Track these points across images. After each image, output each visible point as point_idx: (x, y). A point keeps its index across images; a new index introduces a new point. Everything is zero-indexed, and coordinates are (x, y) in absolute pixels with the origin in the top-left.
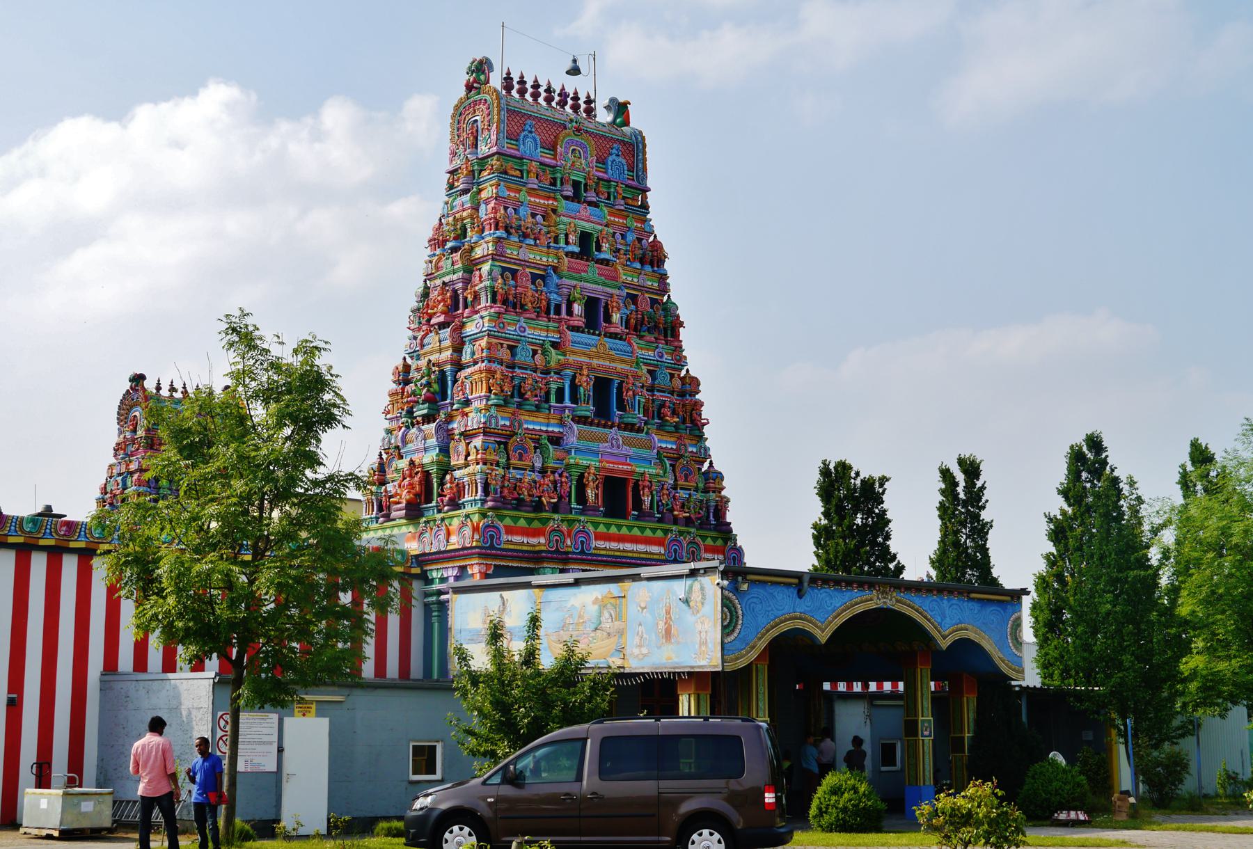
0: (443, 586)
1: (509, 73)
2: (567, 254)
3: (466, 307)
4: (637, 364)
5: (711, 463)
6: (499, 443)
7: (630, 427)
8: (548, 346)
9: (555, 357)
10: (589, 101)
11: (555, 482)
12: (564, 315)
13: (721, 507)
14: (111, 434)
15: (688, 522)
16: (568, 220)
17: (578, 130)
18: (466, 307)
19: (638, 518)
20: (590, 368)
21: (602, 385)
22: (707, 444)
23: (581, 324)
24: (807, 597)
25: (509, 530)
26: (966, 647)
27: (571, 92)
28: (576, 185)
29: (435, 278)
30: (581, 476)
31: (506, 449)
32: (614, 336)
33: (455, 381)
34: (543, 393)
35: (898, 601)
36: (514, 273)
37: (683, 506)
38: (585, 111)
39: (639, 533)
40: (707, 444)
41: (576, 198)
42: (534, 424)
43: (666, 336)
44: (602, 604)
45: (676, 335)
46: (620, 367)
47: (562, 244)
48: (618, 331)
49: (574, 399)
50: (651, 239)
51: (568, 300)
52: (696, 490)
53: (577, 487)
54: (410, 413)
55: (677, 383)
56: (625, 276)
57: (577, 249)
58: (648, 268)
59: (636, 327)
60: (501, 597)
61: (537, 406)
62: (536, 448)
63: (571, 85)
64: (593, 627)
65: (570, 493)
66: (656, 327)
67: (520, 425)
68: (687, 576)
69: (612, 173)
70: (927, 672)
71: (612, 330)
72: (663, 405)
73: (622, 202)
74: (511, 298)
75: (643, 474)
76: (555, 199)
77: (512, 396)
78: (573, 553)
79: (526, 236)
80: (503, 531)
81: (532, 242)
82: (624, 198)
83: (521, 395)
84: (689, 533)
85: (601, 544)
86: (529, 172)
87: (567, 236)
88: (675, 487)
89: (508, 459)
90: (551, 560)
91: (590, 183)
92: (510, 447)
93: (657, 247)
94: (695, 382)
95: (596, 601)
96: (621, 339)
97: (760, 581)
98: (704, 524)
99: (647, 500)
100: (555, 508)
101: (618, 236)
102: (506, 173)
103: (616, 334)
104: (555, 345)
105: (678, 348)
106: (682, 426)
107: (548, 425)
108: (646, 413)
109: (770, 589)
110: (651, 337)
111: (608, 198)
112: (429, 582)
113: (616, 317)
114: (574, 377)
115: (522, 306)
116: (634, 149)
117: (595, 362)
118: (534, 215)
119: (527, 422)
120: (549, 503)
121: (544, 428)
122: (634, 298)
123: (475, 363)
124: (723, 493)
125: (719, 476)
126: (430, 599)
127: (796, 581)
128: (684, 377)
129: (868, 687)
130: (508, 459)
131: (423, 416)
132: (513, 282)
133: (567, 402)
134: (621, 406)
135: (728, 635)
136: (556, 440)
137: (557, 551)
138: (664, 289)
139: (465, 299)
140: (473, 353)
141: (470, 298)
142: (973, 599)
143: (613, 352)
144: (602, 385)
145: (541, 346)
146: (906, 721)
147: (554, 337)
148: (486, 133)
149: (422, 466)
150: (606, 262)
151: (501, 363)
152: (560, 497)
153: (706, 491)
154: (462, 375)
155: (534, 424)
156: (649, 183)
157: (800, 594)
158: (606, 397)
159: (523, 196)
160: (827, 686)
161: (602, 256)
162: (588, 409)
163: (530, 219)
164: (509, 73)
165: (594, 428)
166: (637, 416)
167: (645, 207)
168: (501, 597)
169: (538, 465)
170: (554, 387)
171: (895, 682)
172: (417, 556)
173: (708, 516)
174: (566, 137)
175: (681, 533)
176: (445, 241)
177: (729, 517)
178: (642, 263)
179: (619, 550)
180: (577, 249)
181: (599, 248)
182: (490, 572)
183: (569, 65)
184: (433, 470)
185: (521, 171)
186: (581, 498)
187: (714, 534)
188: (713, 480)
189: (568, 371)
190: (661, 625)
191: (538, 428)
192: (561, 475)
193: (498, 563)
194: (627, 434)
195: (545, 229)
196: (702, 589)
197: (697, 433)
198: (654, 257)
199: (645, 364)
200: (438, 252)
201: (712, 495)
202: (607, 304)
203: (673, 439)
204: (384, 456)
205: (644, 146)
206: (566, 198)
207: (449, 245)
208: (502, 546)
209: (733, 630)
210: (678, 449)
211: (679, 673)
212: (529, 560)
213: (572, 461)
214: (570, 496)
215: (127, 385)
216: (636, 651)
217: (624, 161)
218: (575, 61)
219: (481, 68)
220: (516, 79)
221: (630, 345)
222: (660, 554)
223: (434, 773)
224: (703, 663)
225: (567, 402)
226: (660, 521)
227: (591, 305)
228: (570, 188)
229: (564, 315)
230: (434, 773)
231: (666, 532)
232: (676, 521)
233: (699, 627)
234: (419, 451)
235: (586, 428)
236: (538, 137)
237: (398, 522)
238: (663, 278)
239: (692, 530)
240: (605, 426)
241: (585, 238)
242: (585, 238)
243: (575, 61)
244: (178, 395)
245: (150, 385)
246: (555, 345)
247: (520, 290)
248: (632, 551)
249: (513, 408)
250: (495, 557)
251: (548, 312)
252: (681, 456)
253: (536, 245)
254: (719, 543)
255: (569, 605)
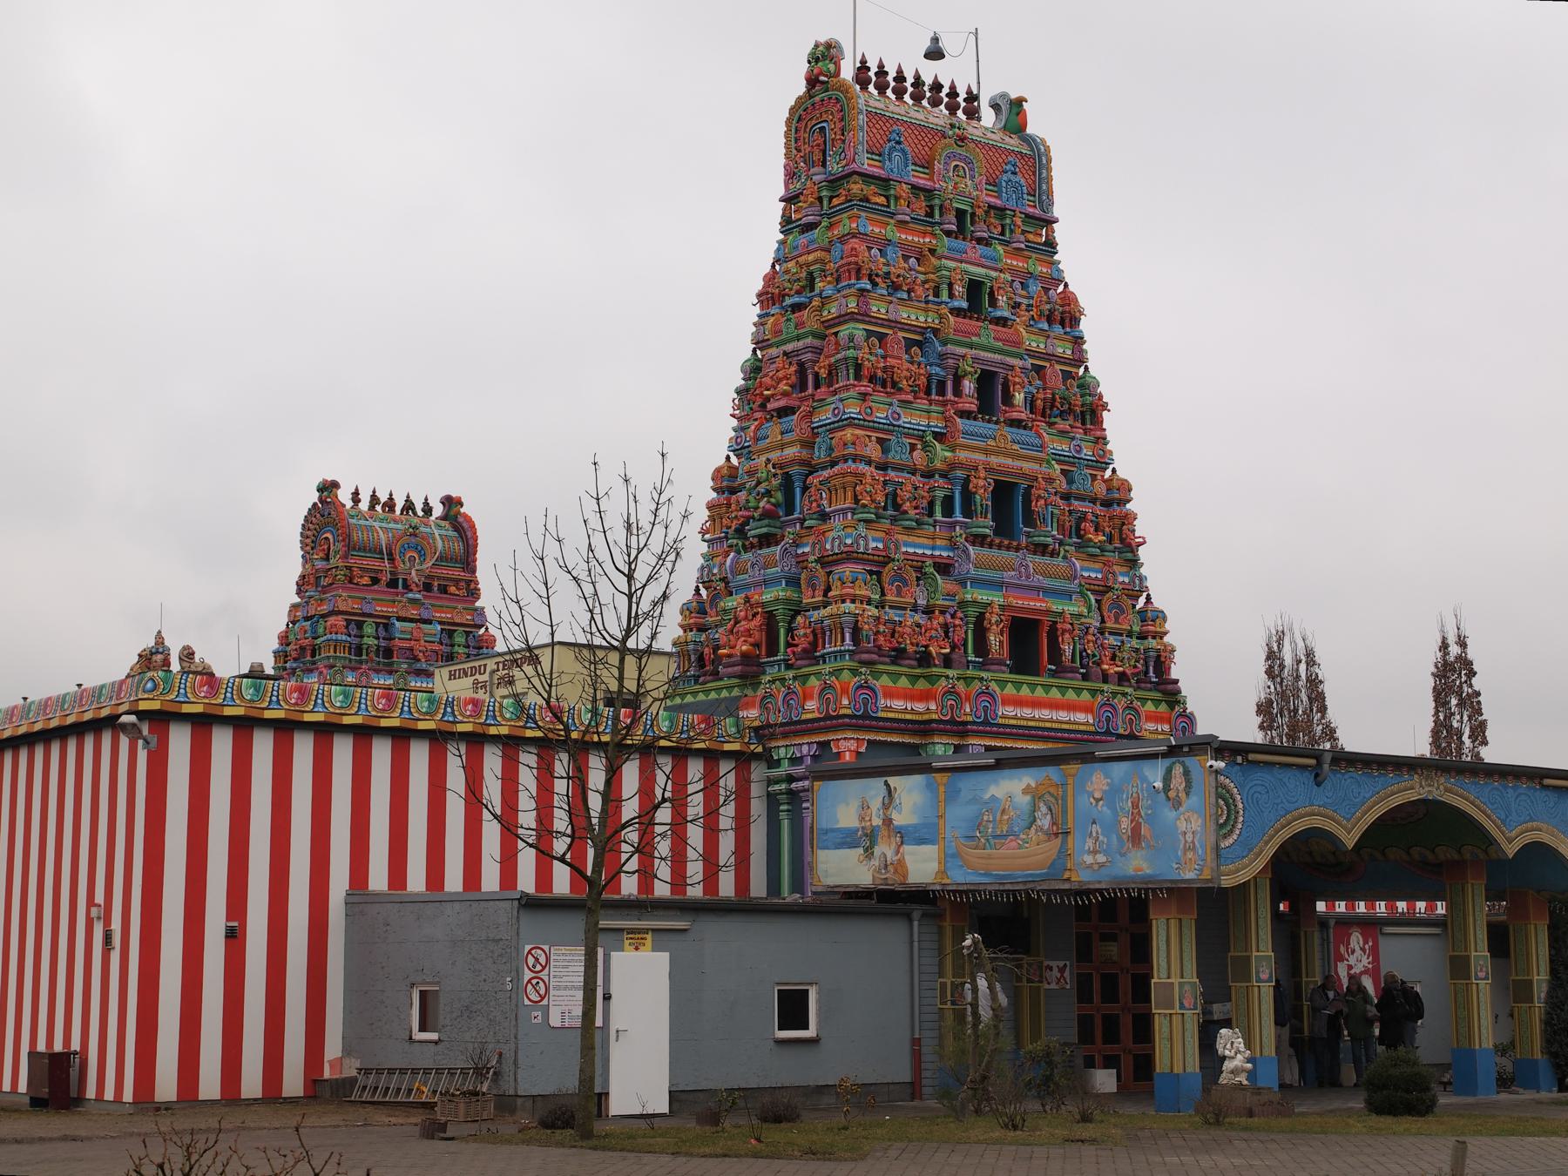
0: (799, 770)
1: (863, 62)
2: (952, 311)
3: (817, 386)
4: (1048, 462)
5: (1148, 598)
6: (871, 573)
7: (1041, 549)
8: (929, 438)
9: (942, 452)
10: (972, 98)
11: (945, 627)
12: (950, 396)
13: (1161, 662)
14: (292, 564)
15: (1122, 678)
16: (952, 264)
17: (962, 139)
18: (817, 386)
19: (1054, 674)
20: (989, 470)
21: (1003, 491)
22: (1143, 571)
23: (974, 408)
24: (1328, 784)
25: (889, 694)
26: (1537, 852)
27: (928, 80)
28: (960, 214)
29: (770, 346)
30: (981, 618)
31: (879, 581)
32: (1016, 423)
33: (805, 489)
34: (925, 503)
35: (1447, 790)
36: (881, 337)
37: (1113, 658)
38: (912, 97)
39: (1059, 696)
40: (1143, 571)
41: (960, 232)
42: (914, 546)
43: (1084, 423)
44: (1036, 795)
45: (1098, 422)
46: (1027, 466)
47: (945, 296)
48: (1023, 416)
49: (968, 511)
50: (1061, 288)
51: (956, 375)
52: (1130, 635)
53: (974, 631)
54: (741, 532)
55: (1100, 489)
56: (1034, 343)
57: (965, 305)
58: (1058, 329)
59: (1048, 410)
60: (886, 783)
61: (917, 521)
62: (918, 579)
63: (929, 71)
64: (1024, 824)
65: (966, 640)
66: (1071, 411)
67: (897, 548)
68: (1164, 755)
69: (1006, 200)
70: (1481, 891)
71: (1015, 415)
72: (1083, 518)
73: (1022, 238)
74: (880, 374)
75: (1061, 614)
76: (933, 235)
77: (885, 508)
78: (974, 723)
79: (895, 287)
80: (880, 695)
81: (905, 296)
82: (1024, 232)
83: (897, 507)
84: (1124, 694)
85: (1010, 711)
86: (897, 198)
87: (950, 286)
88: (1102, 631)
89: (883, 594)
90: (944, 732)
91: (979, 212)
92: (886, 579)
93: (1069, 299)
94: (1126, 487)
95: (1026, 791)
96: (1025, 428)
97: (1266, 763)
98: (1141, 681)
99: (1067, 649)
100: (947, 662)
101: (1017, 285)
102: (868, 200)
103: (1020, 421)
104: (939, 437)
105: (1101, 440)
106: (1110, 547)
107: (933, 548)
108: (1061, 528)
109: (1276, 770)
110: (1063, 425)
111: (1003, 234)
112: (773, 764)
113: (1019, 398)
114: (967, 481)
115: (894, 384)
116: (1033, 163)
117: (994, 460)
118: (906, 258)
119: (906, 545)
120: (939, 654)
121: (929, 552)
122: (1039, 370)
123: (833, 464)
124: (1166, 639)
125: (1160, 616)
126: (777, 787)
127: (1313, 762)
128: (1110, 480)
129: (1373, 908)
130: (883, 594)
131: (760, 536)
132: (880, 351)
133: (958, 516)
134: (1029, 519)
135: (1225, 837)
136: (944, 568)
137: (986, 723)
138: (1079, 359)
139: (816, 375)
140: (831, 449)
141: (823, 373)
142: (1547, 787)
143: (1016, 447)
144: (1003, 491)
145: (921, 438)
146: (1452, 958)
147: (938, 424)
148: (839, 144)
149: (763, 605)
150: (1002, 322)
151: (869, 463)
152: (953, 647)
153: (1142, 637)
154: (814, 480)
155: (914, 546)
156: (1057, 211)
157: (1318, 780)
158: (1009, 504)
159: (892, 232)
160: (1321, 906)
161: (999, 314)
162: (985, 526)
163: (903, 264)
164: (863, 62)
165: (995, 552)
166: (1049, 533)
167: (1051, 245)
168: (886, 783)
169: (922, 602)
170: (940, 494)
171: (1431, 898)
172: (756, 729)
173: (1147, 672)
174: (946, 148)
175: (1114, 694)
176: (783, 296)
177: (1175, 673)
178: (1050, 320)
179: (1033, 719)
180: (965, 305)
181: (993, 302)
182: (862, 750)
183: (926, 44)
184: (780, 610)
185: (887, 198)
186: (981, 647)
187: (1158, 695)
188: (1152, 622)
189: (959, 473)
190: (1125, 823)
191: (920, 551)
192: (953, 616)
193: (872, 737)
194: (1038, 559)
195: (922, 277)
196: (1186, 773)
197: (1129, 556)
198: (1066, 315)
199: (1059, 462)
200: (775, 310)
201: (1152, 643)
202: (1006, 379)
203: (1097, 566)
204: (703, 592)
205: (1049, 160)
206: (948, 233)
207: (788, 301)
208: (1001, 721)
209: (1231, 831)
210: (1105, 578)
211: (1154, 890)
212: (914, 733)
213: (969, 597)
214: (965, 645)
215: (314, 497)
216: (1089, 859)
217: (1023, 181)
218: (935, 40)
219: (825, 54)
220: (910, 80)
221: (1040, 436)
222: (1087, 724)
223: (806, 1027)
224: (1190, 875)
225: (958, 516)
226: (1085, 677)
227: (986, 380)
228: (954, 220)
229: (950, 396)
230: (806, 1027)
231: (1093, 692)
232: (1105, 678)
233: (1182, 825)
234: (757, 585)
235: (986, 551)
236: (908, 149)
237: (726, 682)
238: (1078, 341)
239: (1129, 690)
240: (1008, 548)
241: (974, 287)
242: (974, 287)
243: (935, 40)
244: (364, 505)
245: (344, 496)
246: (939, 437)
247: (891, 362)
248: (1051, 721)
249: (886, 524)
250: (869, 729)
251: (928, 393)
252: (1110, 589)
253: (910, 299)
254: (1163, 708)
255: (987, 796)
